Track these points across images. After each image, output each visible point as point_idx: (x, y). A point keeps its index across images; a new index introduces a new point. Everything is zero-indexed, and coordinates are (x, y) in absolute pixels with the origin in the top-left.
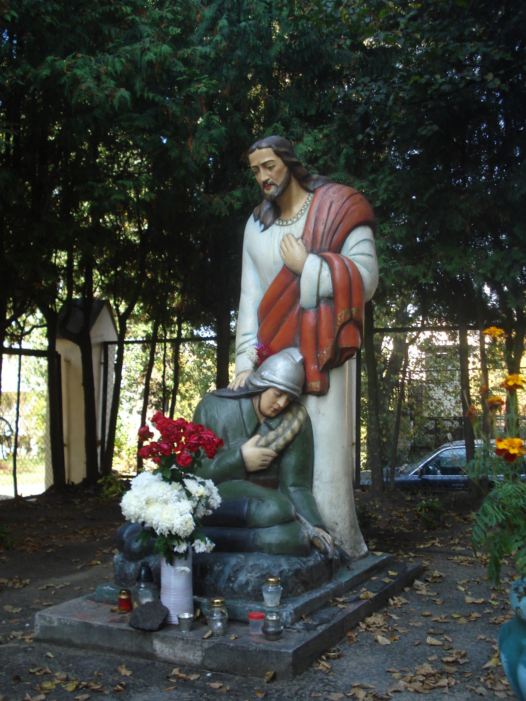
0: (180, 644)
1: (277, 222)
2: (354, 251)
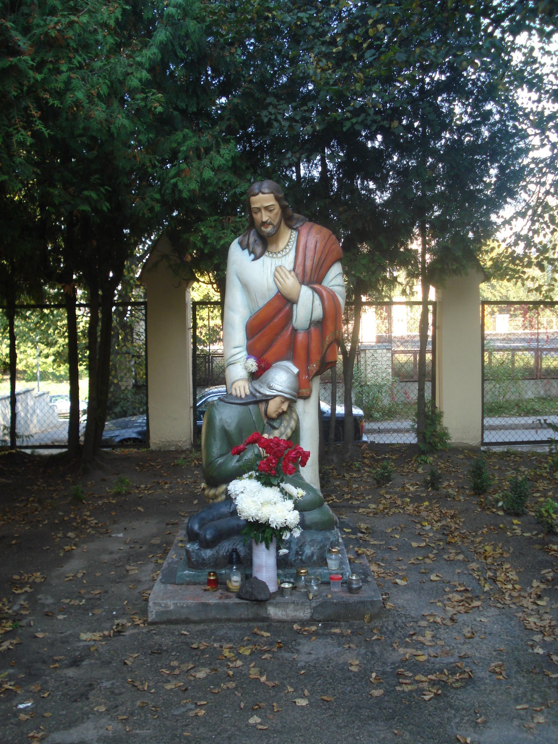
0: (291, 607)
1: (267, 254)
2: (333, 283)
